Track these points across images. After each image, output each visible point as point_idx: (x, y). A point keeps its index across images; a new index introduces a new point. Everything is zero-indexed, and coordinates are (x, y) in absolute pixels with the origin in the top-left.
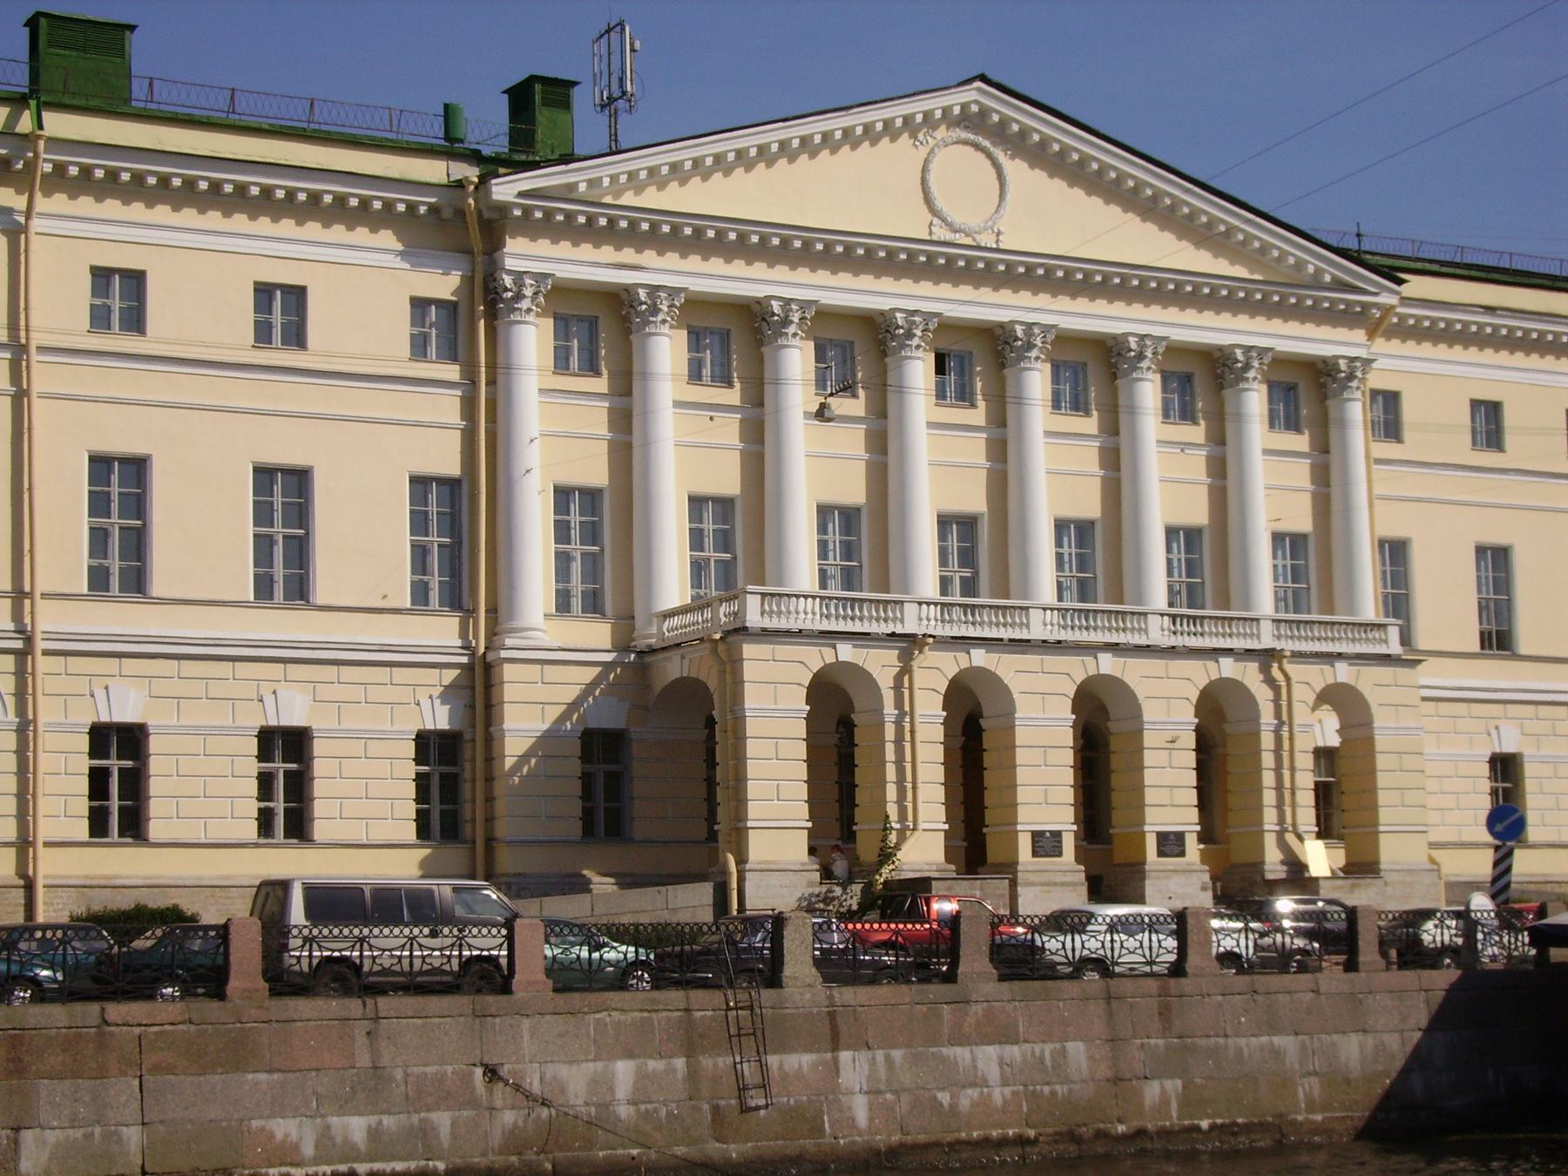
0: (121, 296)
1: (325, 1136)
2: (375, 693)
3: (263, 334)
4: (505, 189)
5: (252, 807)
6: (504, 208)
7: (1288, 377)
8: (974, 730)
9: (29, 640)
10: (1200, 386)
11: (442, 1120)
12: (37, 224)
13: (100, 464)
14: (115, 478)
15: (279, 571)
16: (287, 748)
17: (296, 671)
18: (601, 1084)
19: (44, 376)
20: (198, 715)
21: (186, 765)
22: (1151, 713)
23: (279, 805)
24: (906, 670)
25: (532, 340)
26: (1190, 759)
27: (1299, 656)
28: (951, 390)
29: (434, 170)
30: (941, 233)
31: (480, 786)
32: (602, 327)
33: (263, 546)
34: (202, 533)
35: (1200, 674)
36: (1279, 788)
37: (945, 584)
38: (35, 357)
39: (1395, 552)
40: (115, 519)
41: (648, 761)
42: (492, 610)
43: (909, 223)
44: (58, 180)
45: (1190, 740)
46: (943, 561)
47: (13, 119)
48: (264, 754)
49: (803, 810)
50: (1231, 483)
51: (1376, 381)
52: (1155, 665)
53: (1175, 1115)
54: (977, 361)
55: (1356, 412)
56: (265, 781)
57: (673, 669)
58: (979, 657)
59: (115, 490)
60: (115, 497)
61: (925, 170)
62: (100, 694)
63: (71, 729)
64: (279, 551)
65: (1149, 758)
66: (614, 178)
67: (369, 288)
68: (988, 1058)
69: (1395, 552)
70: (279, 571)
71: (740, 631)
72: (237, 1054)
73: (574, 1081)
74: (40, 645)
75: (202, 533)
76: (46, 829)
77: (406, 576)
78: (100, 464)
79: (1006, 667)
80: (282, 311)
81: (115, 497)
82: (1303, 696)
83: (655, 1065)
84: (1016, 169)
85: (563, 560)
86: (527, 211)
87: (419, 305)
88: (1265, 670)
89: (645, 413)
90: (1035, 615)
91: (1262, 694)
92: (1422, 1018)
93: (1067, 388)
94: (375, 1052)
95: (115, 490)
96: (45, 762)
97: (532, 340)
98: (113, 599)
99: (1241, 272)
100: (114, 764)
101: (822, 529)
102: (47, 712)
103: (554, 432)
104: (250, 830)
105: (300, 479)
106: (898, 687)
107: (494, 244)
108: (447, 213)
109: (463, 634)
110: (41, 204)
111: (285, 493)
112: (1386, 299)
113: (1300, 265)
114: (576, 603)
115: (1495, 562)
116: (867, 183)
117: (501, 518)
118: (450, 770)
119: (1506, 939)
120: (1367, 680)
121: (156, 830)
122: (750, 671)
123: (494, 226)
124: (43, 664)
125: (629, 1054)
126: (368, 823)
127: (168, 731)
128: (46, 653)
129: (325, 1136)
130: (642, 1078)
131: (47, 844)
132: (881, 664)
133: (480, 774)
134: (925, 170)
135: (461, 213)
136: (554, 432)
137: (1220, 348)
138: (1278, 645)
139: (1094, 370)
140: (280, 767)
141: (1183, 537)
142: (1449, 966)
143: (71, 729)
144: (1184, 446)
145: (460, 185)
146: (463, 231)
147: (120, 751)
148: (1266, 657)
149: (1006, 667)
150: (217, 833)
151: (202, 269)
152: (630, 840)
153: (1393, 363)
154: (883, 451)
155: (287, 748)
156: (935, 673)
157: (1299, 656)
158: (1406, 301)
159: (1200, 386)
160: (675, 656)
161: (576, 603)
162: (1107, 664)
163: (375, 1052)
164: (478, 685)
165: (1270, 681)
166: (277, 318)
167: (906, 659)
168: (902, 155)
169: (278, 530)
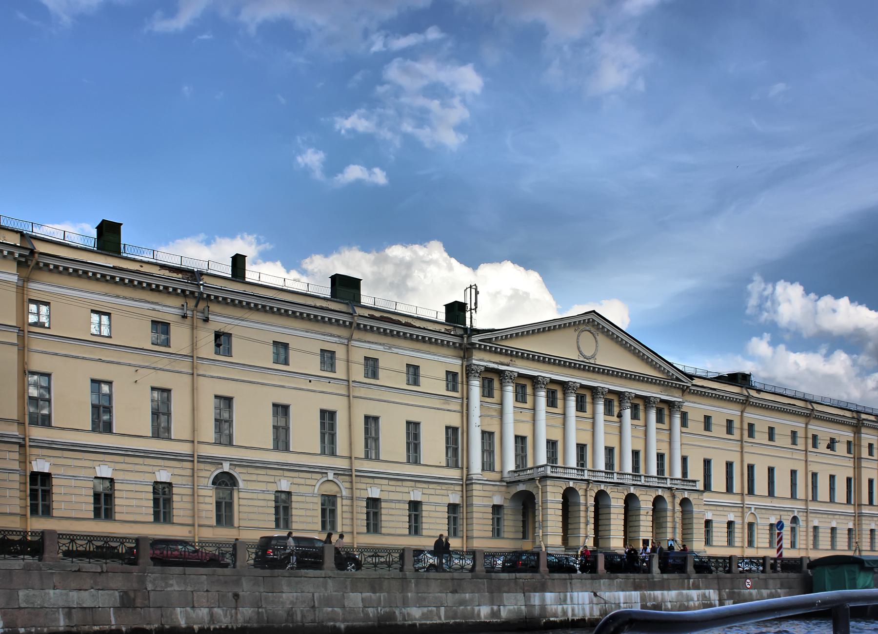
21: (432, 514)
22: (613, 503)
28: (486, 393)
30: (582, 359)
34: (392, 441)
39: (684, 459)
43: (572, 355)
45: (651, 513)
53: (443, 618)
63: (404, 502)
75: (392, 441)
80: (414, 373)
86: (480, 345)
90: (586, 472)
101: (483, 438)
111: (413, 428)
115: (771, 470)
119: (169, 552)
120: (692, 497)
127: (386, 501)
148: (669, 489)
149: (608, 490)
150: (399, 532)
152: (734, 546)
158: (693, 385)
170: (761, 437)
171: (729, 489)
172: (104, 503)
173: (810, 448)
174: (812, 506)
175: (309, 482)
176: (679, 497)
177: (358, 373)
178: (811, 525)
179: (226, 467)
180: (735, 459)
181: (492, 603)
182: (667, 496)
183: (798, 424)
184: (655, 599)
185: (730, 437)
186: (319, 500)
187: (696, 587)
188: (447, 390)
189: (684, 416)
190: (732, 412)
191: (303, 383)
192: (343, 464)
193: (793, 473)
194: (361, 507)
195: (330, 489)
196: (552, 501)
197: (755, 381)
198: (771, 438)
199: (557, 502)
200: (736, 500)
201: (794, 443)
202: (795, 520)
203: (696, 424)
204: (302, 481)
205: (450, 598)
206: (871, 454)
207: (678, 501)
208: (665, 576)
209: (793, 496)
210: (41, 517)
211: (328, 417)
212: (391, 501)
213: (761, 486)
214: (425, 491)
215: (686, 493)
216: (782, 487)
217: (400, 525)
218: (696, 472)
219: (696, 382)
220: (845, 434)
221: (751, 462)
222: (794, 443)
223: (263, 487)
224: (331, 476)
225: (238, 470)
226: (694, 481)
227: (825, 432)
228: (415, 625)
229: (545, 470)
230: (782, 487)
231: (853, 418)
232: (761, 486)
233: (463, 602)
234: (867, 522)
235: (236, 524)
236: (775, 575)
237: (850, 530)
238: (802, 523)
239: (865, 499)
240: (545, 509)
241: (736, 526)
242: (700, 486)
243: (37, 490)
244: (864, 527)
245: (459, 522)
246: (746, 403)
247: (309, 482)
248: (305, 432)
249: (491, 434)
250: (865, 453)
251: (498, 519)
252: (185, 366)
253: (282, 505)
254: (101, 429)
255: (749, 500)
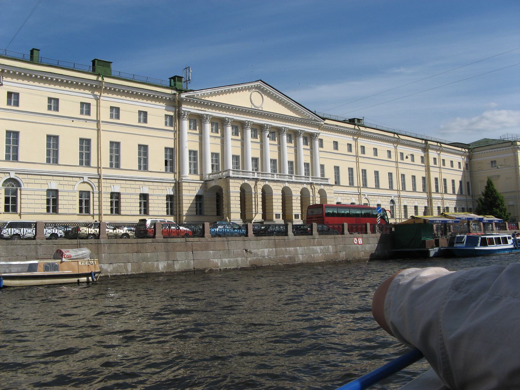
0: (115, 112)
1: (222, 261)
2: (159, 188)
3: (50, 108)
4: (183, 96)
5: (45, 206)
6: (182, 99)
7: (255, 127)
8: (266, 194)
9: (100, 176)
10: (198, 120)
11: (239, 259)
12: (101, 98)
13: (112, 143)
14: (11, 136)
15: (84, 160)
16: (144, 197)
17: (146, 183)
18: (263, 252)
19: (103, 127)
20: (67, 188)
21: (128, 200)
22: (294, 193)
23: (51, 206)
24: (256, 185)
25: (186, 123)
26: (299, 202)
27: (317, 184)
29: (169, 91)
30: (253, 107)
31: (178, 205)
32: (197, 121)
33: (81, 155)
34: (129, 157)
35: (301, 187)
36: (255, 205)
37: (253, 170)
38: (101, 123)
39: (322, 166)
40: (11, 145)
41: (212, 200)
42: (179, 173)
43: (248, 105)
44: (106, 90)
45: (299, 198)
46: (190, 160)
47: (98, 78)
48: (111, 198)
49: (240, 210)
50: (281, 152)
51: (320, 137)
52: (294, 185)
54: (240, 127)
55: (317, 143)
56: (112, 202)
57: (213, 184)
58: (267, 183)
59: (11, 138)
60: (11, 140)
61: (251, 96)
62: (112, 187)
63: (136, 194)
64: (84, 156)
65: (293, 201)
66: (201, 94)
67: (158, 112)
68: (318, 248)
69: (322, 166)
70: (84, 160)
71: (228, 177)
72: (207, 248)
73: (259, 251)
74: (102, 177)
75: (129, 157)
76: (104, 212)
77: (45, 157)
78: (112, 143)
79: (271, 184)
80: (143, 116)
81: (11, 140)
82: (317, 191)
83: (270, 249)
84: (265, 97)
85: (190, 164)
86: (186, 99)
87: (166, 116)
88: (311, 186)
89: (205, 139)
91: (310, 190)
92: (377, 242)
93: (192, 124)
94: (228, 247)
95: (11, 138)
96: (103, 200)
97: (186, 123)
98: (114, 169)
99: (297, 116)
100: (84, 199)
102: (103, 190)
103: (190, 141)
104: (45, 211)
105: (56, 138)
106: (255, 188)
107: (180, 106)
108: (172, 99)
109: (175, 177)
110: (102, 94)
111: (143, 150)
112: (322, 123)
113: (309, 116)
114: (114, 166)
116: (240, 99)
117: (314, 170)
118: (173, 202)
120: (326, 188)
121: (60, 211)
122: (231, 184)
123: (180, 102)
124: (103, 181)
125: (267, 248)
126: (158, 210)
127: (124, 194)
128: (103, 179)
129: (222, 261)
130: (269, 251)
131: (104, 215)
132: (252, 184)
133: (178, 203)
134: (251, 96)
135: (174, 100)
136: (190, 141)
137: (243, 121)
138: (259, 177)
139: (276, 132)
140: (143, 201)
141: (215, 155)
142: (125, 238)
143: (136, 194)
144: (290, 147)
145: (175, 94)
146: (175, 104)
147: (116, 197)
148: (311, 184)
149: (271, 184)
151: (130, 108)
153: (323, 135)
154: (223, 143)
155: (144, 197)
156: (260, 185)
157: (317, 184)
159: (309, 140)
160: (214, 182)
161: (114, 166)
162: (287, 185)
163: (228, 247)
164: (178, 186)
165: (312, 188)
166: (84, 109)
167: (256, 182)
168: (247, 93)
169: (84, 152)
170: (448, 165)
171: (351, 184)
172: (53, 202)
173: (360, 154)
174: (403, 194)
175: (70, 183)
176: (318, 188)
177: (105, 115)
178: (403, 204)
179: (13, 175)
180: (393, 171)
181: (168, 260)
182: (308, 187)
183: (390, 147)
184: (290, 252)
185: (350, 153)
186: (78, 194)
187: (320, 244)
188: (166, 125)
189: (321, 141)
190: (349, 139)
191: (68, 122)
192: (94, 172)
193: (390, 174)
194: (136, 200)
195: (86, 188)
196: (234, 192)
197: (366, 122)
198: (376, 154)
199: (279, 195)
200: (355, 190)
201: (390, 156)
202: (392, 201)
203: (328, 146)
204: (66, 183)
205: (135, 257)
206: (435, 163)
207: (317, 191)
208: (297, 237)
209: (391, 188)
210: (51, 214)
211: (85, 143)
212: (128, 194)
213: (371, 182)
214: (151, 187)
215: (322, 186)
216: (384, 182)
217: (133, 208)
218: (330, 174)
219: (327, 121)
220: (419, 153)
221: (322, 163)
222: (390, 156)
223: (38, 187)
224: (86, 179)
225: (21, 176)
226: (327, 179)
227: (407, 151)
228: (107, 276)
229: (229, 173)
230: (384, 182)
231: (437, 146)
232: (371, 182)
233: (144, 259)
234: (435, 202)
235: (91, 213)
236: (373, 235)
237: (425, 207)
238: (397, 204)
239: (433, 189)
240: (229, 196)
241: (205, 199)
242: (332, 181)
243: (9, 198)
244: (434, 205)
245: (175, 206)
246: (357, 134)
247: (70, 183)
248: (69, 152)
249: (89, 141)
250: (431, 163)
251: (200, 204)
252: (94, 125)
253: (84, 199)
254: (11, 160)
255: (363, 190)
